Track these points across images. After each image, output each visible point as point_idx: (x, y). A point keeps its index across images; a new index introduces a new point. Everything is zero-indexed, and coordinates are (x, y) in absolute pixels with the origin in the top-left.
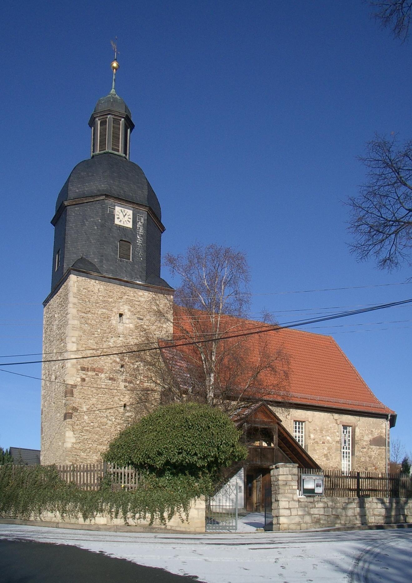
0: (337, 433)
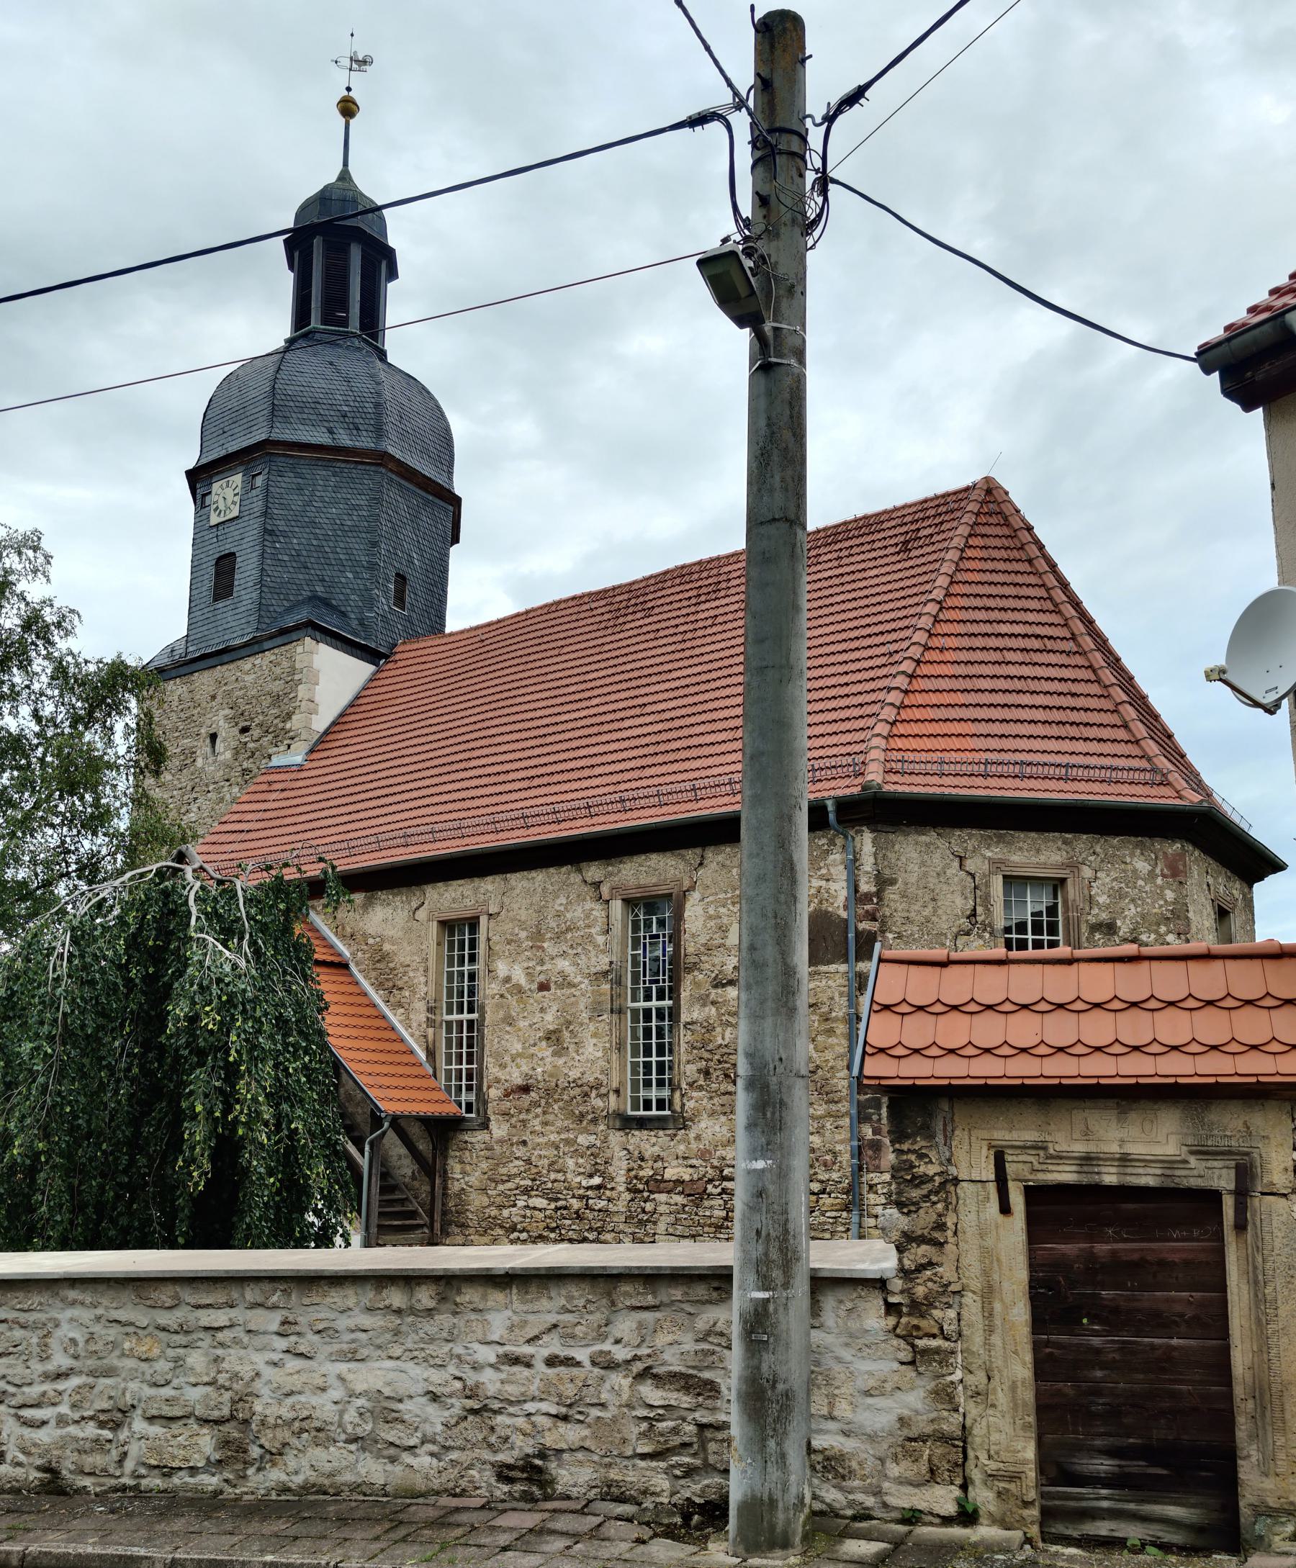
0: (600, 939)
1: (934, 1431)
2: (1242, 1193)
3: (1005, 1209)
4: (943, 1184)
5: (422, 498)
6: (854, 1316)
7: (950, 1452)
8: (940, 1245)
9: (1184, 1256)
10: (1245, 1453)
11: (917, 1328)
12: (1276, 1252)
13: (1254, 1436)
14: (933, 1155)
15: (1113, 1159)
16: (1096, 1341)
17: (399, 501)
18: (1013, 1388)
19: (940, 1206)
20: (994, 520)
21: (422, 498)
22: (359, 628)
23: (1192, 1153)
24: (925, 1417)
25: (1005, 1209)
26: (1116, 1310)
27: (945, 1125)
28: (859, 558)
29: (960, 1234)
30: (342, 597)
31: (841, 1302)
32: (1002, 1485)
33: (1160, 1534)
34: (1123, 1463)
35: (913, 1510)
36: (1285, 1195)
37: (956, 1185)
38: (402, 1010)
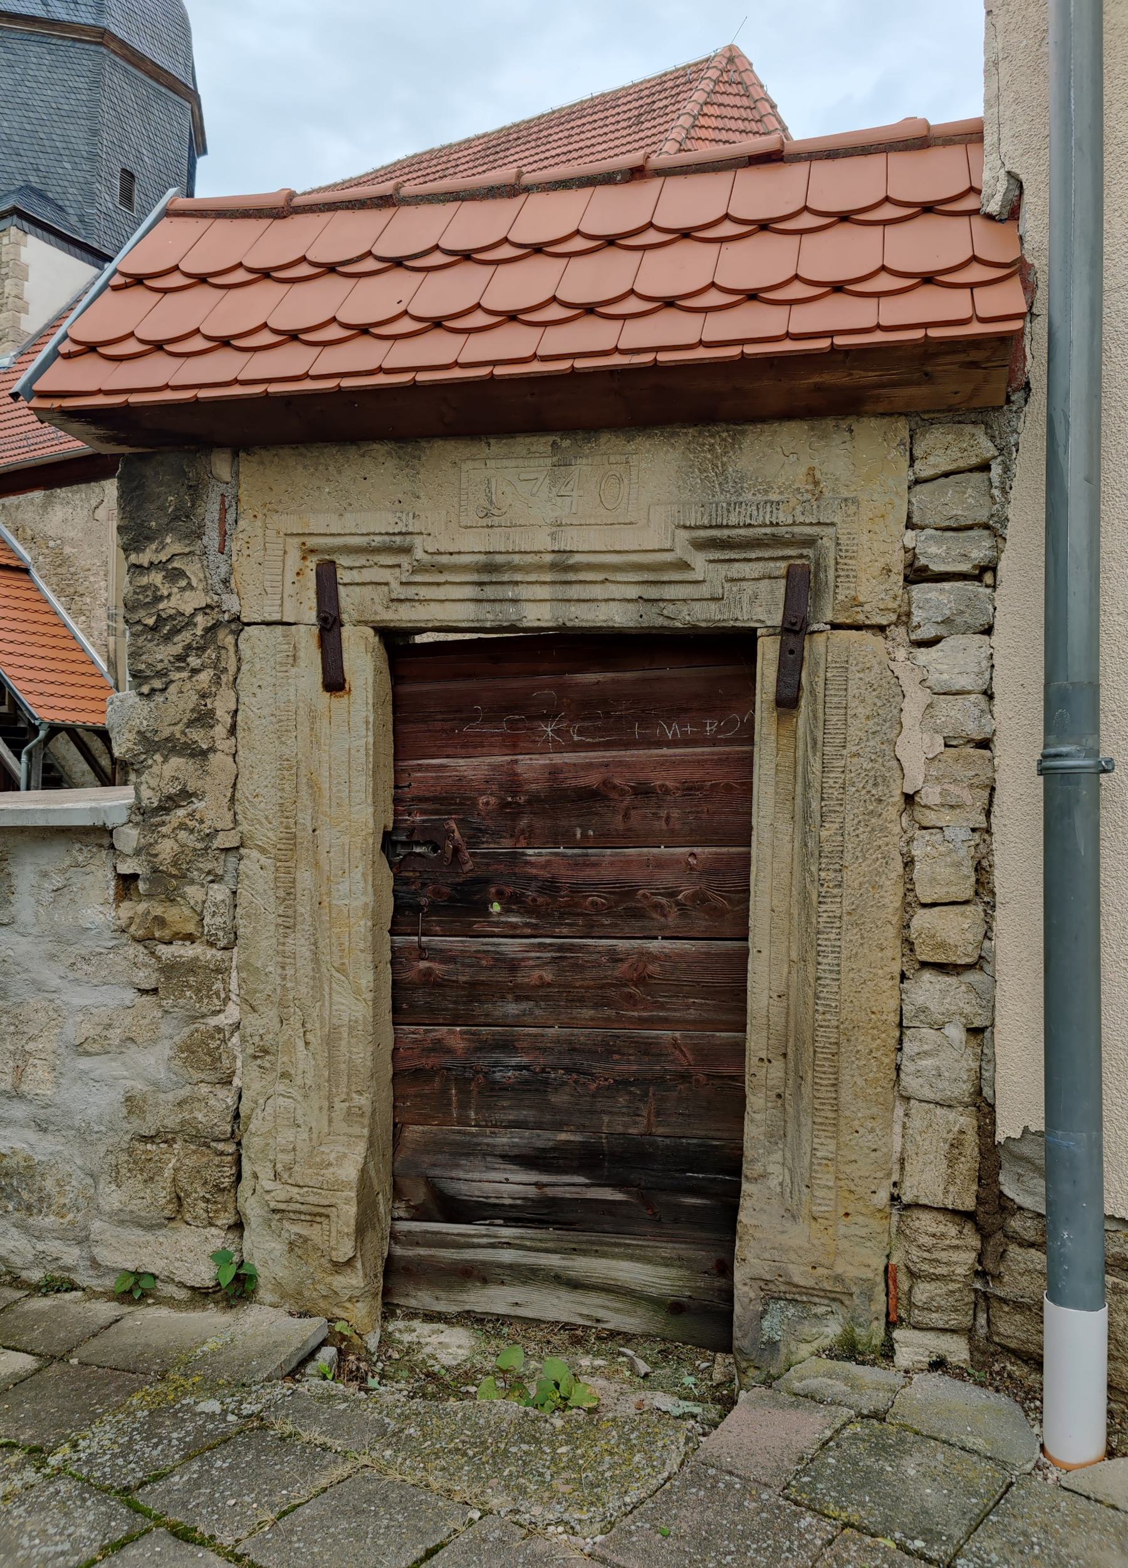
1: (183, 1123)
2: (794, 630)
3: (334, 682)
4: (211, 630)
5: (154, 89)
6: (65, 901)
7: (207, 1165)
8: (201, 754)
9: (685, 774)
10: (758, 1168)
11: (160, 922)
12: (852, 748)
13: (777, 1136)
14: (193, 570)
15: (540, 568)
16: (511, 946)
17: (121, 82)
18: (331, 1041)
19: (205, 677)
20: (734, 89)
21: (154, 89)
22: (79, 225)
23: (701, 545)
24: (170, 1097)
25: (334, 682)
26: (550, 886)
27: (224, 511)
28: (589, 135)
29: (240, 733)
30: (59, 189)
31: (45, 875)
32: (296, 1228)
33: (601, 1314)
34: (545, 1178)
35: (137, 1275)
36: (882, 629)
37: (237, 633)
38: (83, 618)
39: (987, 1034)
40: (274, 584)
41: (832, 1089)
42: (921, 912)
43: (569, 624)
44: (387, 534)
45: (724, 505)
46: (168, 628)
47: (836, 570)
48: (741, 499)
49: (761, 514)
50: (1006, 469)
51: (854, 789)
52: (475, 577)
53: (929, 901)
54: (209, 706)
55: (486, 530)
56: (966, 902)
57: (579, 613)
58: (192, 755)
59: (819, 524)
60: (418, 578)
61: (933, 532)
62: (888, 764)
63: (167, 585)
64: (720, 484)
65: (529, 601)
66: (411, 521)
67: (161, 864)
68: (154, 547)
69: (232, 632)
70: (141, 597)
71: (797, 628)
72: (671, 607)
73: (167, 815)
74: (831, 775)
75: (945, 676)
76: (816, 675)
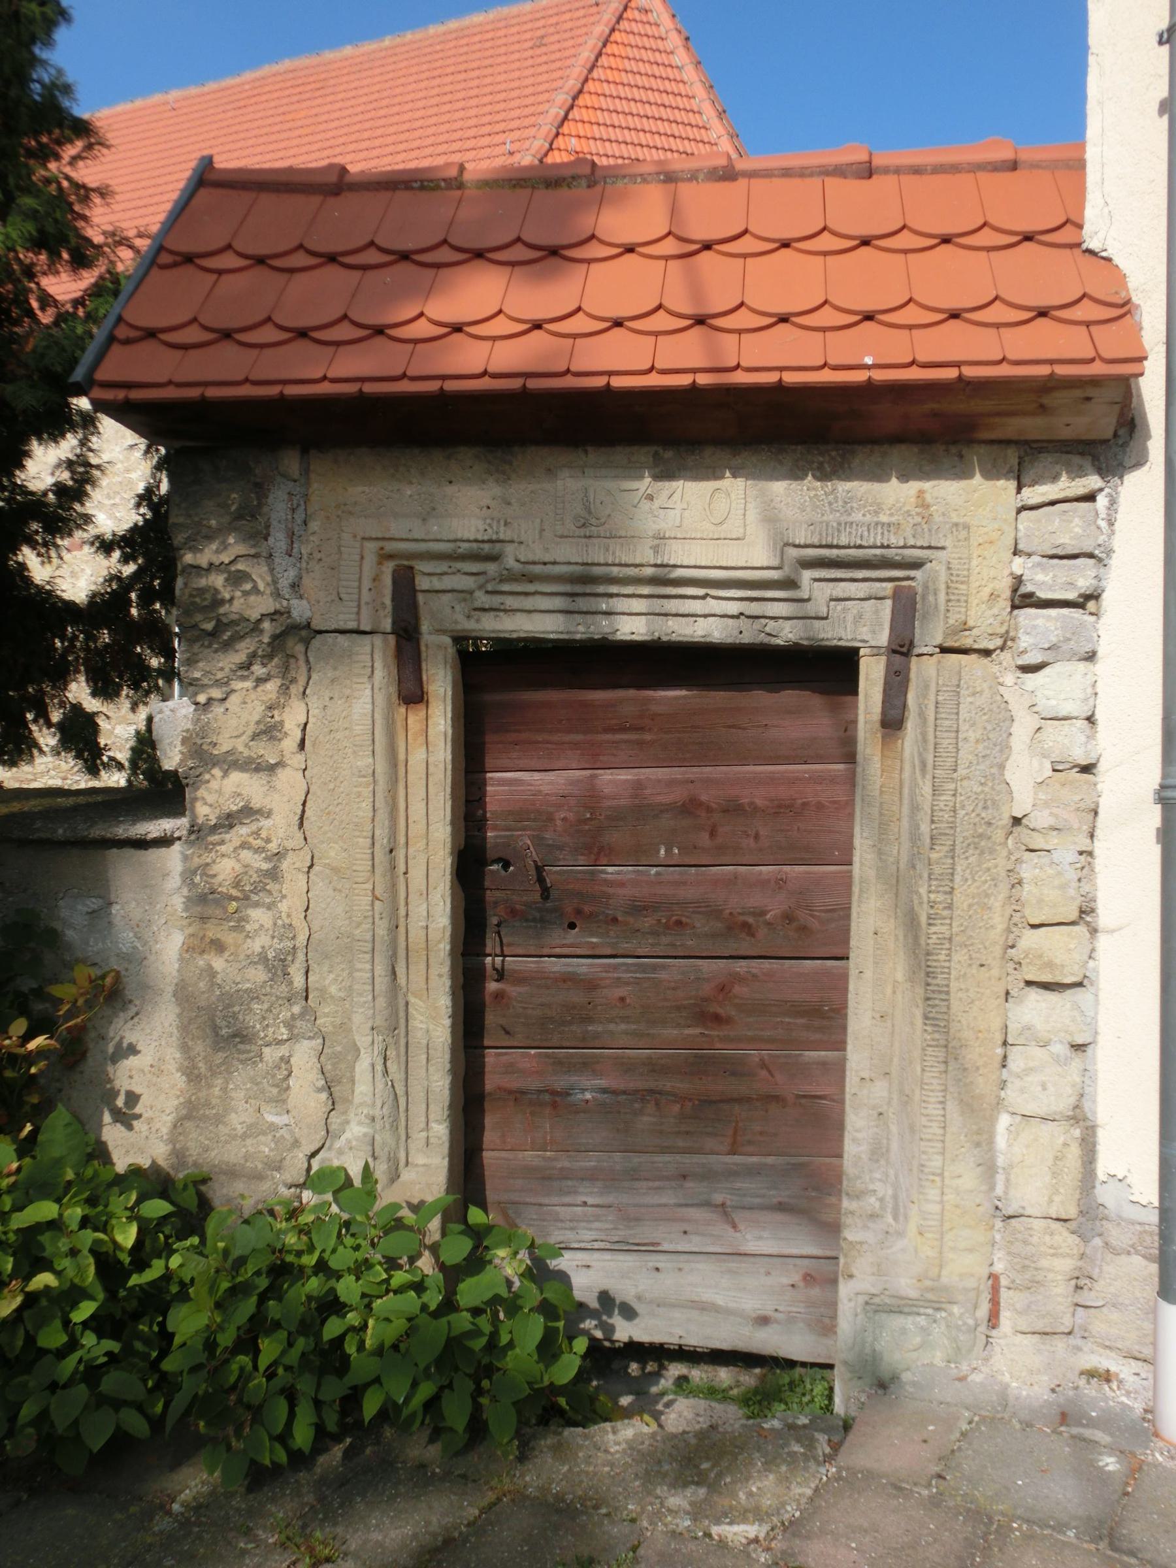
2: (901, 649)
12: (962, 771)
36: (987, 653)
37: (307, 643)
39: (1090, 1050)
40: (350, 590)
41: (940, 1106)
42: (1030, 933)
43: (665, 638)
44: (476, 541)
45: (835, 525)
46: (229, 634)
47: (947, 594)
48: (850, 519)
49: (872, 535)
50: (1113, 502)
51: (964, 812)
52: (567, 588)
53: (1037, 922)
54: (277, 718)
55: (584, 540)
56: (1073, 923)
57: (676, 628)
58: (257, 770)
59: (930, 547)
60: (506, 587)
61: (1039, 559)
62: (998, 788)
63: (229, 589)
64: (830, 504)
65: (624, 614)
66: (502, 529)
67: (220, 885)
68: (214, 546)
69: (302, 640)
70: (198, 600)
71: (904, 650)
72: (772, 623)
73: (227, 833)
74: (942, 798)
75: (1053, 702)
76: (925, 696)
